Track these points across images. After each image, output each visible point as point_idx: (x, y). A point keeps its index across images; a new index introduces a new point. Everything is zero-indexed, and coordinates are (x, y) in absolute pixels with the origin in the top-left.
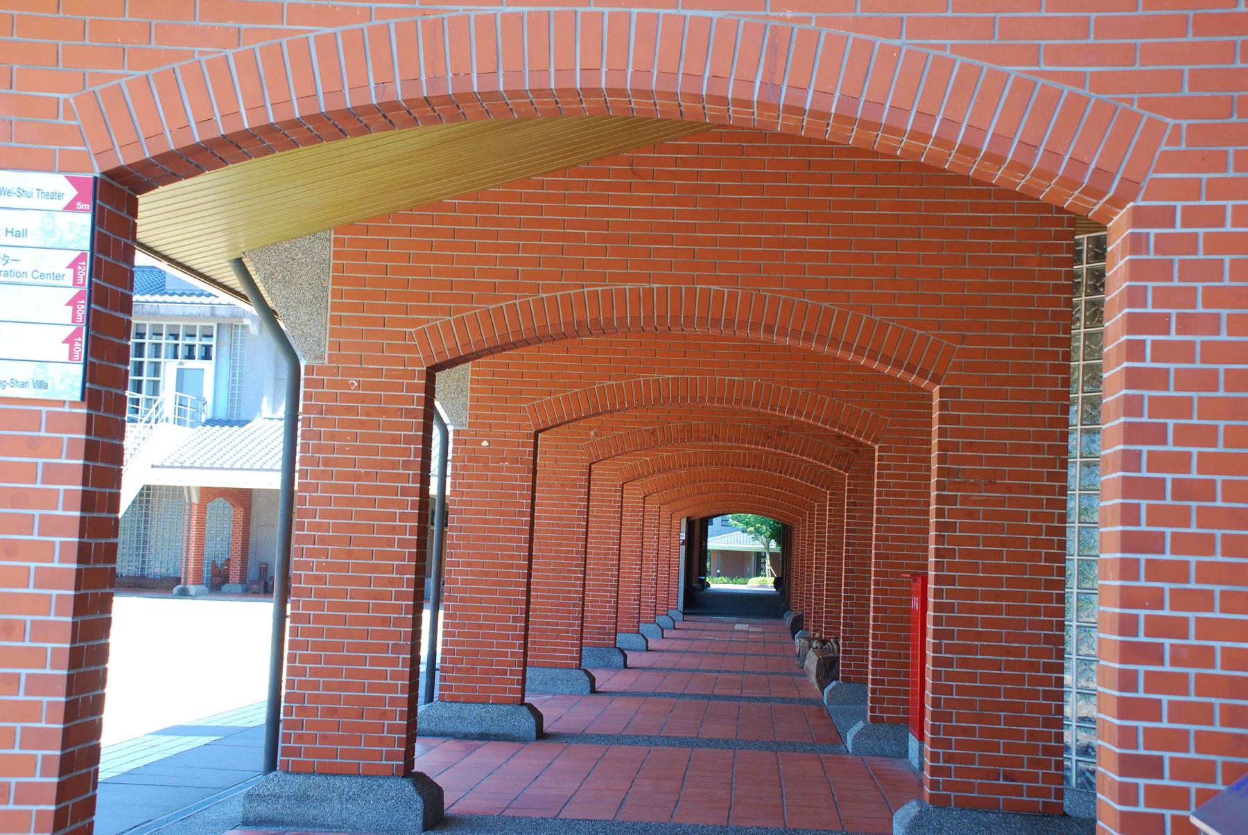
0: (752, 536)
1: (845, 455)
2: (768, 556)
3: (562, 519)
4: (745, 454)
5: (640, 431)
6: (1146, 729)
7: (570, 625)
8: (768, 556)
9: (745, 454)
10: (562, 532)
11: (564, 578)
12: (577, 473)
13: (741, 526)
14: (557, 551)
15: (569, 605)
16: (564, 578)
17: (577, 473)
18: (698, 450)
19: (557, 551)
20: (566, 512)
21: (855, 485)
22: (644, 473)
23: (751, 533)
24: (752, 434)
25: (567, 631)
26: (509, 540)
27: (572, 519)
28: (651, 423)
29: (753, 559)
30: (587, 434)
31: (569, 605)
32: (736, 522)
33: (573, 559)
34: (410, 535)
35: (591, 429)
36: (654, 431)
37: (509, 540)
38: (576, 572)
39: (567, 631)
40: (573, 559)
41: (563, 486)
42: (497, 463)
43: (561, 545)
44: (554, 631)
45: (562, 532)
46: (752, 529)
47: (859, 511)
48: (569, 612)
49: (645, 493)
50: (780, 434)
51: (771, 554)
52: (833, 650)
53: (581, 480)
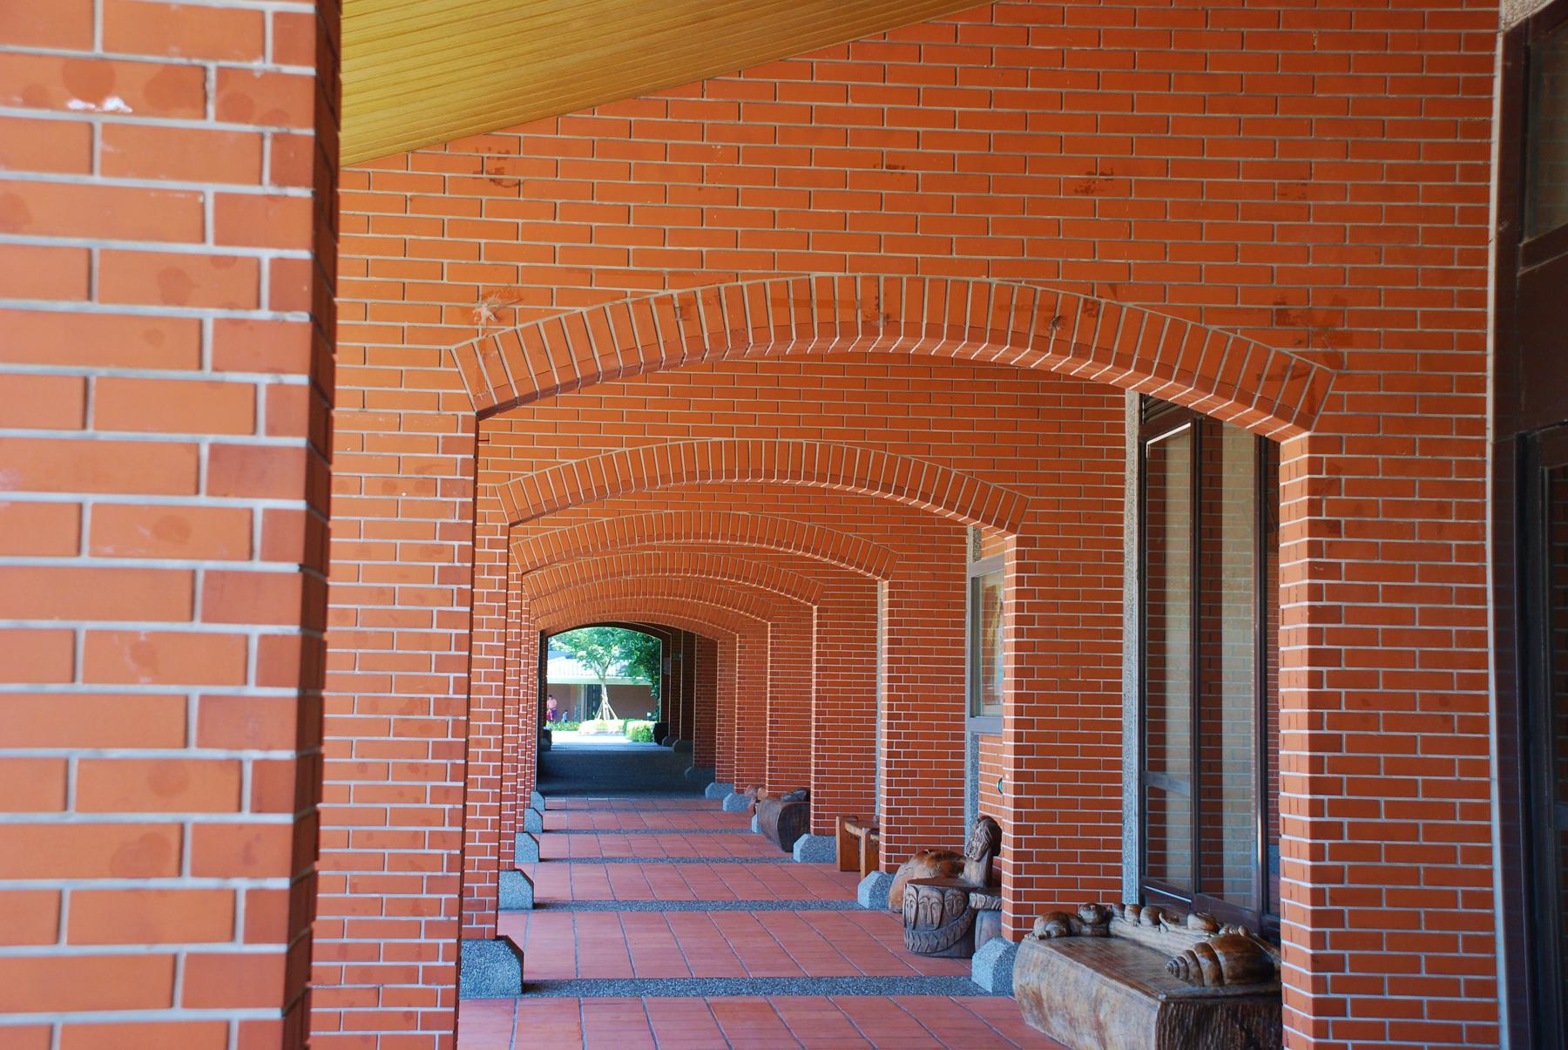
0: (584, 662)
1: (1301, 373)
2: (604, 690)
3: (387, 596)
4: (811, 448)
5: (642, 303)
6: (1459, 996)
7: (421, 952)
8: (604, 690)
9: (811, 448)
10: (388, 640)
11: (400, 794)
12: (435, 445)
13: (567, 649)
14: (374, 706)
15: (415, 885)
16: (400, 794)
17: (435, 445)
18: (697, 440)
19: (374, 706)
20: (403, 575)
21: (1334, 467)
22: (562, 497)
23: (581, 658)
24: (1003, 308)
25: (411, 975)
26: (148, 656)
27: (420, 597)
28: (679, 279)
29: (583, 695)
30: (468, 315)
31: (415, 885)
32: (560, 644)
33: (426, 728)
34: (263, 682)
35: (479, 296)
36: (688, 304)
37: (148, 656)
38: (441, 773)
39: (411, 975)
40: (426, 728)
41: (390, 487)
42: (33, 98)
43: (387, 684)
44: (366, 975)
45: (388, 640)
46: (584, 653)
47: (1347, 549)
48: (416, 908)
49: (523, 566)
50: (1091, 309)
51: (609, 687)
52: (1200, 974)
53: (450, 466)
